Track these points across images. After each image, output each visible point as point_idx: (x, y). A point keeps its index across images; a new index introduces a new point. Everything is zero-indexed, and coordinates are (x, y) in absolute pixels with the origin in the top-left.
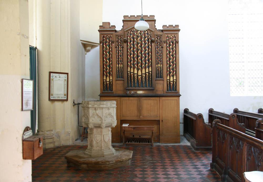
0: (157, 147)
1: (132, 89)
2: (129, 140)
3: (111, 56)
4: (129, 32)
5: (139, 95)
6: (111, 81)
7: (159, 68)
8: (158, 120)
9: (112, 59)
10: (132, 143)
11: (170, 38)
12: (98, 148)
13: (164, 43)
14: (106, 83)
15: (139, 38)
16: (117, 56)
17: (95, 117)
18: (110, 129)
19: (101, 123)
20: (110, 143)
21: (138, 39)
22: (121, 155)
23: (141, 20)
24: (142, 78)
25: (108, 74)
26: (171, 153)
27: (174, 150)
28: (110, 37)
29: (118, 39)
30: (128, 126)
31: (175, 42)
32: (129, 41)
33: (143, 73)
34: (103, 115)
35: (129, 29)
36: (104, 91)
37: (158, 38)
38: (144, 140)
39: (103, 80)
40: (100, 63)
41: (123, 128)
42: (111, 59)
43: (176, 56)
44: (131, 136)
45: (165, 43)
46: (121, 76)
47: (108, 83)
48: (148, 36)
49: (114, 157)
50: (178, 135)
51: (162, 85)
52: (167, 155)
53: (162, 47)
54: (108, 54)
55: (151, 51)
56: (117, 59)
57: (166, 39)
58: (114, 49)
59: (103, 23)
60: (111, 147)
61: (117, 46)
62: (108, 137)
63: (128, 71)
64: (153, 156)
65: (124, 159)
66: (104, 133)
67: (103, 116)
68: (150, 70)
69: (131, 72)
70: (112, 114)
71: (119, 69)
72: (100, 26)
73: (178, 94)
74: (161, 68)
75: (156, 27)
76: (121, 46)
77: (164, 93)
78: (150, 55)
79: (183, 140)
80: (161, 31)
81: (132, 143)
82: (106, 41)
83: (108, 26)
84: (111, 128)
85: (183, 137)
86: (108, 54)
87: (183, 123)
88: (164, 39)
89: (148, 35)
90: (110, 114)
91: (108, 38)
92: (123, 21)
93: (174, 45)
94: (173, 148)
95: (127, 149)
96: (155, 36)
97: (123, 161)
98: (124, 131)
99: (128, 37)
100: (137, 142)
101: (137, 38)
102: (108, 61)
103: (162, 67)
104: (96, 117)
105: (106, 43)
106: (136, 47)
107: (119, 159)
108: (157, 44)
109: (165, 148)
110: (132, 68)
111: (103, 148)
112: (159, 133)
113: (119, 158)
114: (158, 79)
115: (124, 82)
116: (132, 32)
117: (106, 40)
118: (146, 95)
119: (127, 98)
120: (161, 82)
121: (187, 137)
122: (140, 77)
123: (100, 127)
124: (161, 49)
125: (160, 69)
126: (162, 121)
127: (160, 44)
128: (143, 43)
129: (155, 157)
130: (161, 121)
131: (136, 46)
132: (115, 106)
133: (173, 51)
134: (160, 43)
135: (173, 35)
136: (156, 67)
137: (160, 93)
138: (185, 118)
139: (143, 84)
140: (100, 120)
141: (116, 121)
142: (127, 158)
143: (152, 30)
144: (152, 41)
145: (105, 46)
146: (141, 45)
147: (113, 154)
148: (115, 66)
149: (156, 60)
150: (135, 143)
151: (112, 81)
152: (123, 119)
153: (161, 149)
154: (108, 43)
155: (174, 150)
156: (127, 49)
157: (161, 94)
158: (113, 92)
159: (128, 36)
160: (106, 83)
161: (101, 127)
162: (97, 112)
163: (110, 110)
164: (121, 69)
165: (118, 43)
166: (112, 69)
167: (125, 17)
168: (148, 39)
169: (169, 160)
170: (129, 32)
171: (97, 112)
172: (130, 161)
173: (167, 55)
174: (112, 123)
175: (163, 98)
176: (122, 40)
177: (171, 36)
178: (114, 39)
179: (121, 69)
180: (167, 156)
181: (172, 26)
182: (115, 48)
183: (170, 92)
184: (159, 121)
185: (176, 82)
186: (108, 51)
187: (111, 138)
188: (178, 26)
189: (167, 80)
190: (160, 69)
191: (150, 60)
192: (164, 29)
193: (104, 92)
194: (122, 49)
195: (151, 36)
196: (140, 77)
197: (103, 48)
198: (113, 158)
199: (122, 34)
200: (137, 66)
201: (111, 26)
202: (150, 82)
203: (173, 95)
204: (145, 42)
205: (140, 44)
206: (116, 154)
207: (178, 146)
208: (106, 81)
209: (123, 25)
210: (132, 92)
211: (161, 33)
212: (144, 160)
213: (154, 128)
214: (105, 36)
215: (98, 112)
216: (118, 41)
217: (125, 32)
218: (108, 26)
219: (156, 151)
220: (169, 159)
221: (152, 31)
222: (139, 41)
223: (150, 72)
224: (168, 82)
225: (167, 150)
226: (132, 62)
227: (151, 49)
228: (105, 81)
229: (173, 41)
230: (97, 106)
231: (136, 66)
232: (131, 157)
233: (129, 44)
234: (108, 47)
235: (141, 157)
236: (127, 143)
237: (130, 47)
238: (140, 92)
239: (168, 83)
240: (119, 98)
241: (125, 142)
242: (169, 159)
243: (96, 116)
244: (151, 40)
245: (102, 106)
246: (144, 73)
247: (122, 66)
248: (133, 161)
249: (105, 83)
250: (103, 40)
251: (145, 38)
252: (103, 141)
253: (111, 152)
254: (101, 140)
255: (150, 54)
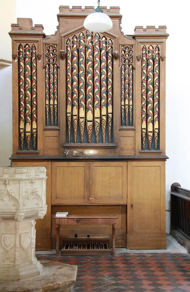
0: (123, 257)
1: (75, 146)
2: (67, 243)
3: (34, 84)
4: (71, 38)
5: (87, 158)
6: (34, 131)
7: (127, 106)
8: (122, 205)
9: (37, 89)
10: (73, 250)
11: (149, 51)
12: (7, 262)
13: (136, 60)
14: (25, 135)
15: (90, 50)
16: (46, 85)
17: (4, 199)
18: (34, 223)
19: (16, 209)
20: (33, 250)
21: (87, 53)
22: (54, 275)
23: (96, 12)
24: (94, 125)
25: (28, 118)
26: (152, 269)
27: (158, 263)
28: (32, 47)
29: (49, 51)
30: (67, 215)
31: (157, 58)
32: (70, 55)
33: (96, 116)
34: (21, 194)
35: (71, 33)
36: (21, 149)
37: (125, 52)
38: (97, 243)
39: (19, 129)
40: (14, 98)
41: (57, 221)
42: (35, 90)
43: (159, 84)
44: (72, 237)
45: (138, 60)
46: (54, 121)
47: (28, 134)
48: (106, 47)
49: (41, 280)
50: (163, 234)
51: (132, 139)
52: (145, 273)
53: (133, 69)
54: (28, 79)
55: (113, 75)
56: (47, 90)
57: (142, 52)
58: (41, 73)
59: (18, 19)
60: (34, 259)
61: (47, 66)
62: (28, 239)
63: (67, 113)
64: (117, 275)
65: (61, 283)
66: (20, 231)
67: (21, 197)
68: (110, 110)
69: (74, 114)
70: (40, 193)
71: (50, 108)
72: (13, 26)
73: (162, 154)
74: (131, 107)
75: (122, 30)
76: (53, 65)
77: (135, 154)
78: (110, 82)
79: (170, 242)
80: (131, 37)
81: (73, 250)
82: (26, 55)
83: (29, 27)
84: (36, 220)
85: (170, 238)
86: (28, 79)
87: (169, 211)
88: (137, 52)
89: (107, 46)
90: (34, 193)
91: (29, 50)
92: (59, 17)
93: (157, 65)
94: (155, 258)
95: (65, 261)
96: (121, 46)
97: (58, 288)
98: (59, 225)
99: (69, 49)
100: (84, 247)
101: (85, 50)
102: (28, 92)
103: (133, 105)
104: (6, 199)
105: (25, 60)
106: (84, 67)
107: (51, 285)
108: (123, 62)
109: (138, 258)
110: (75, 107)
111: (17, 263)
112: (125, 230)
113: (50, 281)
114: (124, 127)
115: (59, 133)
116: (75, 40)
117: (24, 53)
118: (102, 158)
119: (65, 164)
120: (131, 133)
121: (179, 238)
122: (89, 124)
123: (13, 219)
124: (131, 71)
125: (129, 109)
126: (132, 206)
127: (129, 63)
128: (97, 59)
129: (122, 277)
130: (129, 207)
131: (82, 65)
132: (44, 176)
133: (154, 75)
134: (129, 61)
135: (154, 46)
136: (121, 105)
137: (128, 153)
138: (174, 200)
139: (96, 137)
140: (14, 205)
141: (46, 206)
142: (67, 280)
143: (115, 35)
144: (115, 57)
145: (22, 64)
146: (93, 64)
147: (39, 275)
148: (42, 103)
149: (121, 93)
150: (80, 250)
151: (37, 131)
152: (56, 202)
153: (131, 261)
154: (29, 58)
155: (158, 263)
156: (67, 72)
157: (129, 156)
158: (38, 151)
159: (67, 47)
160: (25, 135)
161: (16, 218)
162: (9, 188)
163: (34, 184)
164: (54, 109)
165: (49, 60)
166: (36, 108)
167: (61, 8)
168: (107, 53)
169: (149, 285)
170: (71, 38)
171: (8, 188)
172: (72, 287)
173: (142, 83)
174: (38, 211)
175: (134, 163)
176: (57, 53)
177: (151, 48)
178: (41, 50)
179: (54, 109)
180: (145, 275)
181: (153, 27)
182: (43, 68)
183: (148, 151)
184: (127, 205)
185: (159, 134)
186: (28, 73)
187: (34, 241)
188: (164, 28)
189: (142, 129)
190: (129, 109)
191: (111, 93)
192: (137, 34)
193: (20, 151)
194: (55, 71)
195: (112, 47)
196: (91, 123)
197: (19, 69)
198: (38, 282)
199: (55, 43)
200: (86, 104)
201: (34, 26)
202: (110, 134)
203: (152, 157)
204: (100, 58)
205: (90, 63)
206: (44, 273)
207: (164, 254)
208: (25, 132)
209: (59, 24)
210: (75, 152)
211: (131, 42)
212: (100, 284)
213: (116, 219)
214: (23, 44)
215: (12, 188)
216: (48, 56)
217: (63, 38)
218: (29, 27)
219: (121, 265)
220: (151, 282)
221: (115, 38)
222: (89, 55)
223: (110, 115)
224: (144, 133)
225: (143, 262)
226: (75, 95)
227: (113, 72)
228: (22, 131)
229: (154, 57)
230: (9, 177)
231: (82, 103)
232: (75, 279)
233: (69, 61)
234: (28, 66)
235: (93, 278)
236: (64, 249)
237: (72, 68)
238: (91, 152)
239: (144, 136)
240: (50, 163)
241: (60, 248)
242: (151, 282)
243: (7, 196)
244: (112, 54)
245: (18, 176)
246: (99, 116)
247: (56, 103)
248: (78, 286)
249: (23, 135)
250: (19, 53)
251: (101, 51)
252: (18, 246)
253: (34, 270)
254: (15, 245)
255: (110, 80)
